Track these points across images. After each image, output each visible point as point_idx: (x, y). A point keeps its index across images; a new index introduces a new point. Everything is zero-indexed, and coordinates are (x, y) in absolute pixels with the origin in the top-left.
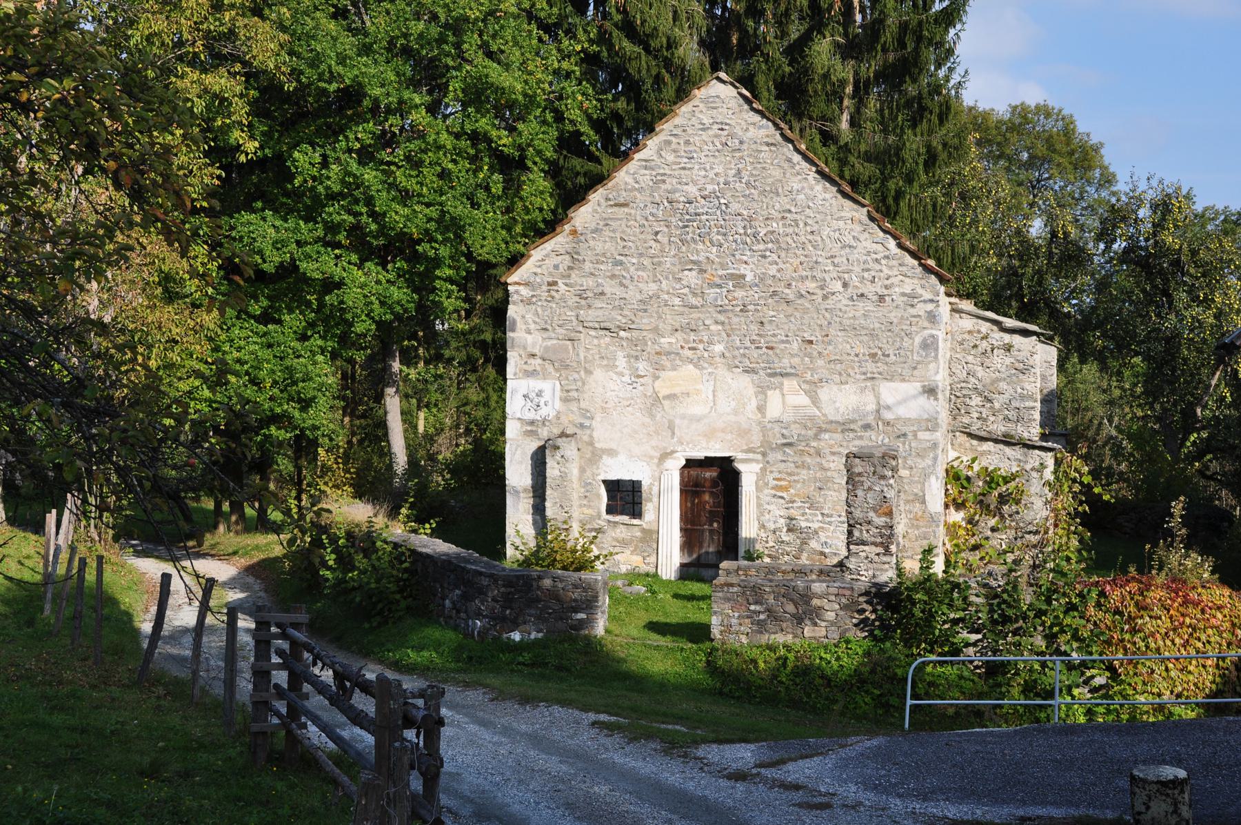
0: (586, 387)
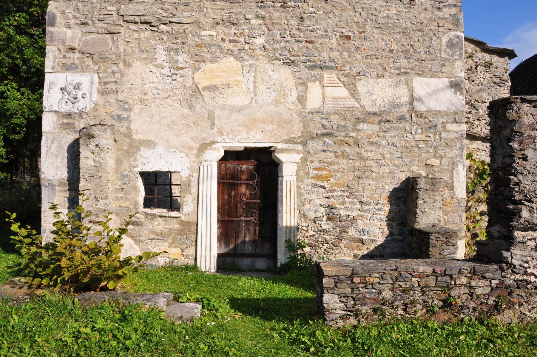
0: (125, 79)
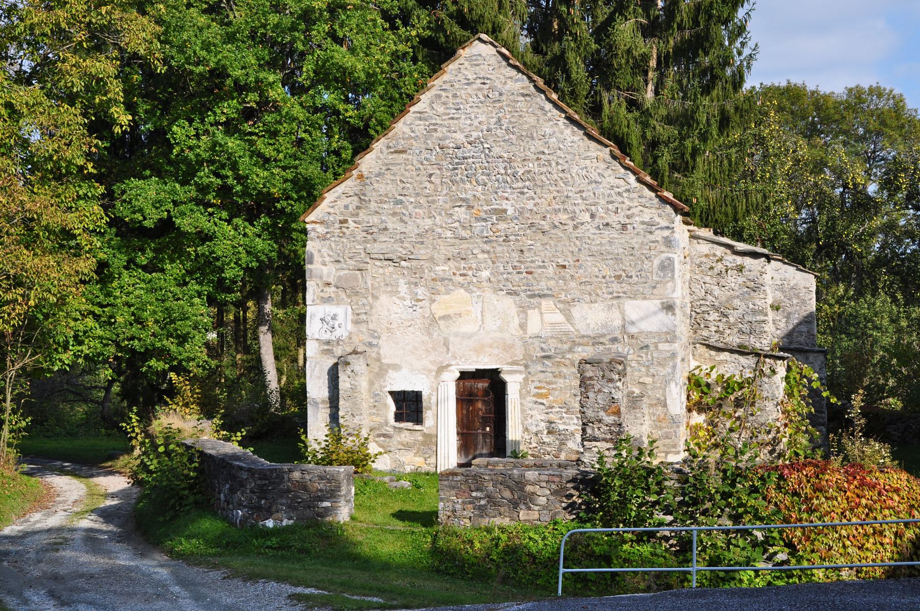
0: (374, 310)
